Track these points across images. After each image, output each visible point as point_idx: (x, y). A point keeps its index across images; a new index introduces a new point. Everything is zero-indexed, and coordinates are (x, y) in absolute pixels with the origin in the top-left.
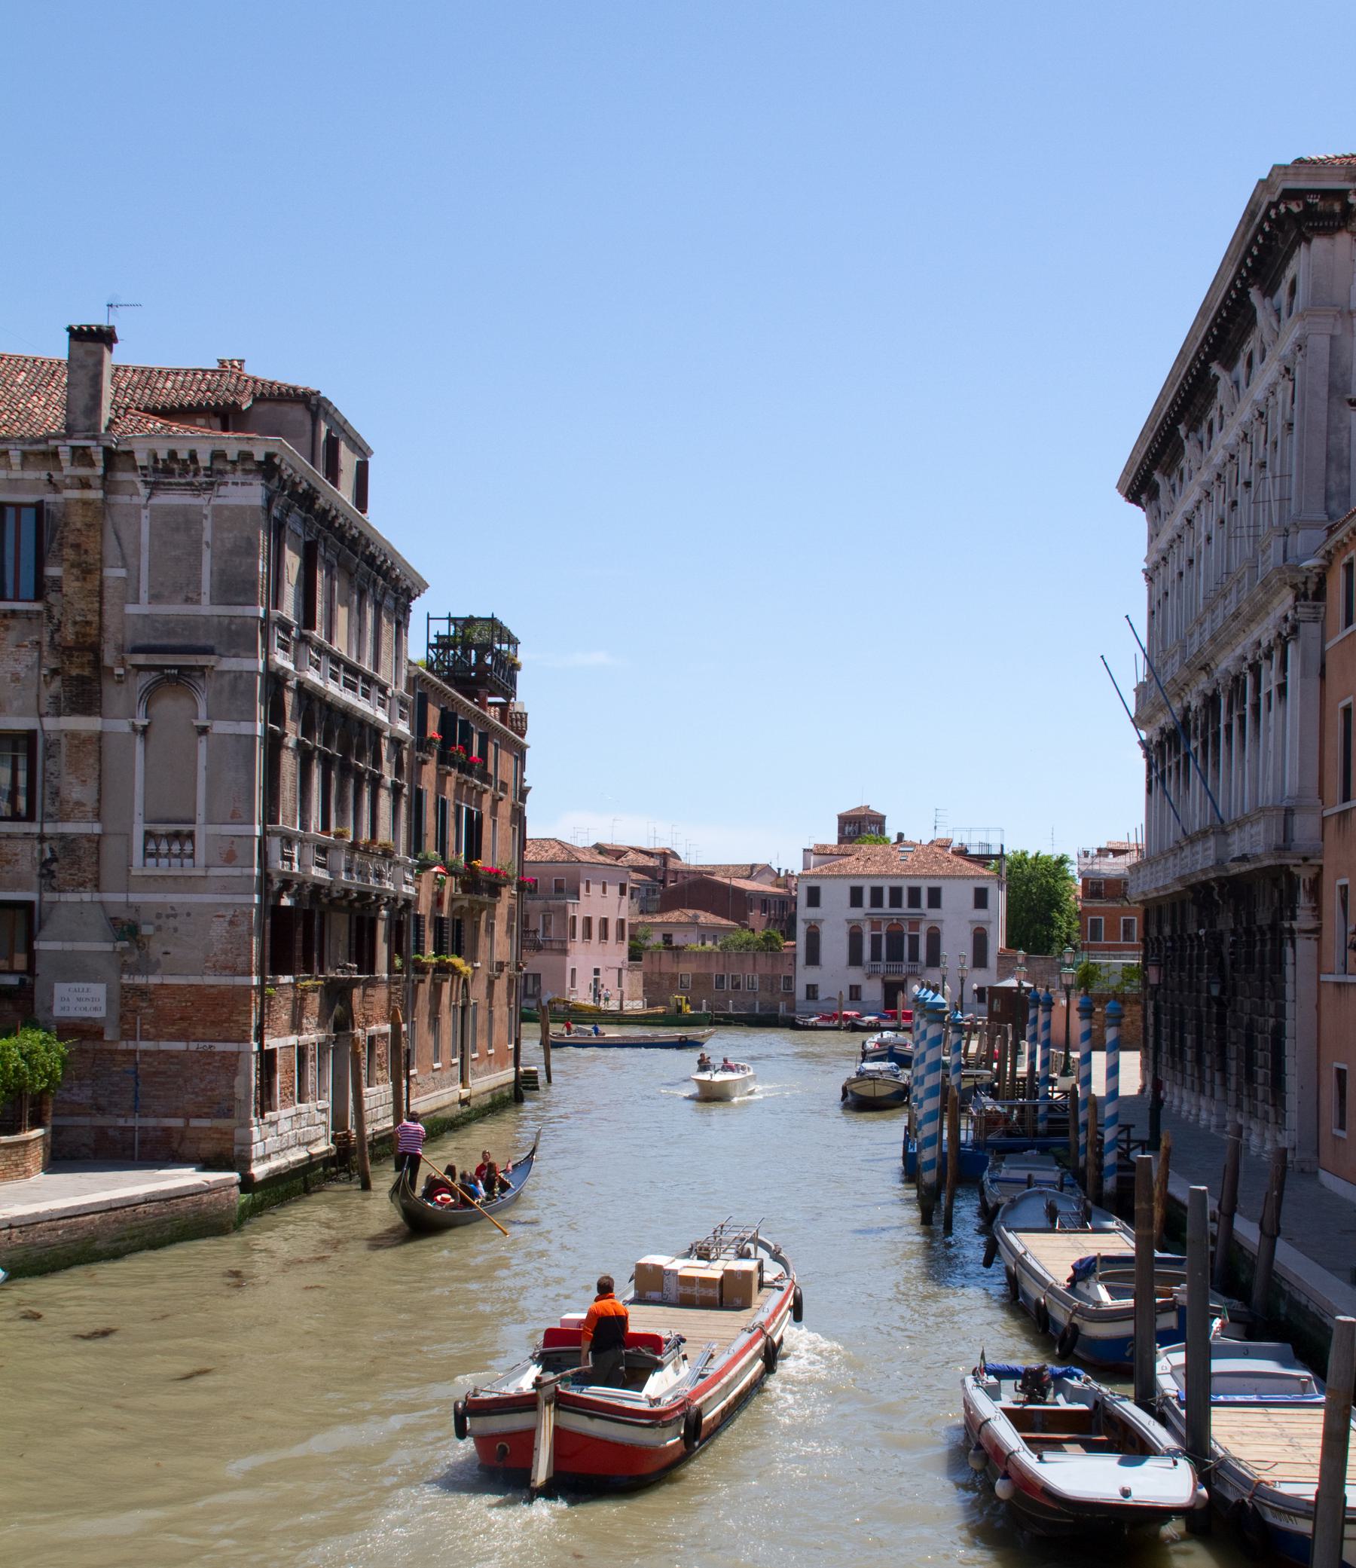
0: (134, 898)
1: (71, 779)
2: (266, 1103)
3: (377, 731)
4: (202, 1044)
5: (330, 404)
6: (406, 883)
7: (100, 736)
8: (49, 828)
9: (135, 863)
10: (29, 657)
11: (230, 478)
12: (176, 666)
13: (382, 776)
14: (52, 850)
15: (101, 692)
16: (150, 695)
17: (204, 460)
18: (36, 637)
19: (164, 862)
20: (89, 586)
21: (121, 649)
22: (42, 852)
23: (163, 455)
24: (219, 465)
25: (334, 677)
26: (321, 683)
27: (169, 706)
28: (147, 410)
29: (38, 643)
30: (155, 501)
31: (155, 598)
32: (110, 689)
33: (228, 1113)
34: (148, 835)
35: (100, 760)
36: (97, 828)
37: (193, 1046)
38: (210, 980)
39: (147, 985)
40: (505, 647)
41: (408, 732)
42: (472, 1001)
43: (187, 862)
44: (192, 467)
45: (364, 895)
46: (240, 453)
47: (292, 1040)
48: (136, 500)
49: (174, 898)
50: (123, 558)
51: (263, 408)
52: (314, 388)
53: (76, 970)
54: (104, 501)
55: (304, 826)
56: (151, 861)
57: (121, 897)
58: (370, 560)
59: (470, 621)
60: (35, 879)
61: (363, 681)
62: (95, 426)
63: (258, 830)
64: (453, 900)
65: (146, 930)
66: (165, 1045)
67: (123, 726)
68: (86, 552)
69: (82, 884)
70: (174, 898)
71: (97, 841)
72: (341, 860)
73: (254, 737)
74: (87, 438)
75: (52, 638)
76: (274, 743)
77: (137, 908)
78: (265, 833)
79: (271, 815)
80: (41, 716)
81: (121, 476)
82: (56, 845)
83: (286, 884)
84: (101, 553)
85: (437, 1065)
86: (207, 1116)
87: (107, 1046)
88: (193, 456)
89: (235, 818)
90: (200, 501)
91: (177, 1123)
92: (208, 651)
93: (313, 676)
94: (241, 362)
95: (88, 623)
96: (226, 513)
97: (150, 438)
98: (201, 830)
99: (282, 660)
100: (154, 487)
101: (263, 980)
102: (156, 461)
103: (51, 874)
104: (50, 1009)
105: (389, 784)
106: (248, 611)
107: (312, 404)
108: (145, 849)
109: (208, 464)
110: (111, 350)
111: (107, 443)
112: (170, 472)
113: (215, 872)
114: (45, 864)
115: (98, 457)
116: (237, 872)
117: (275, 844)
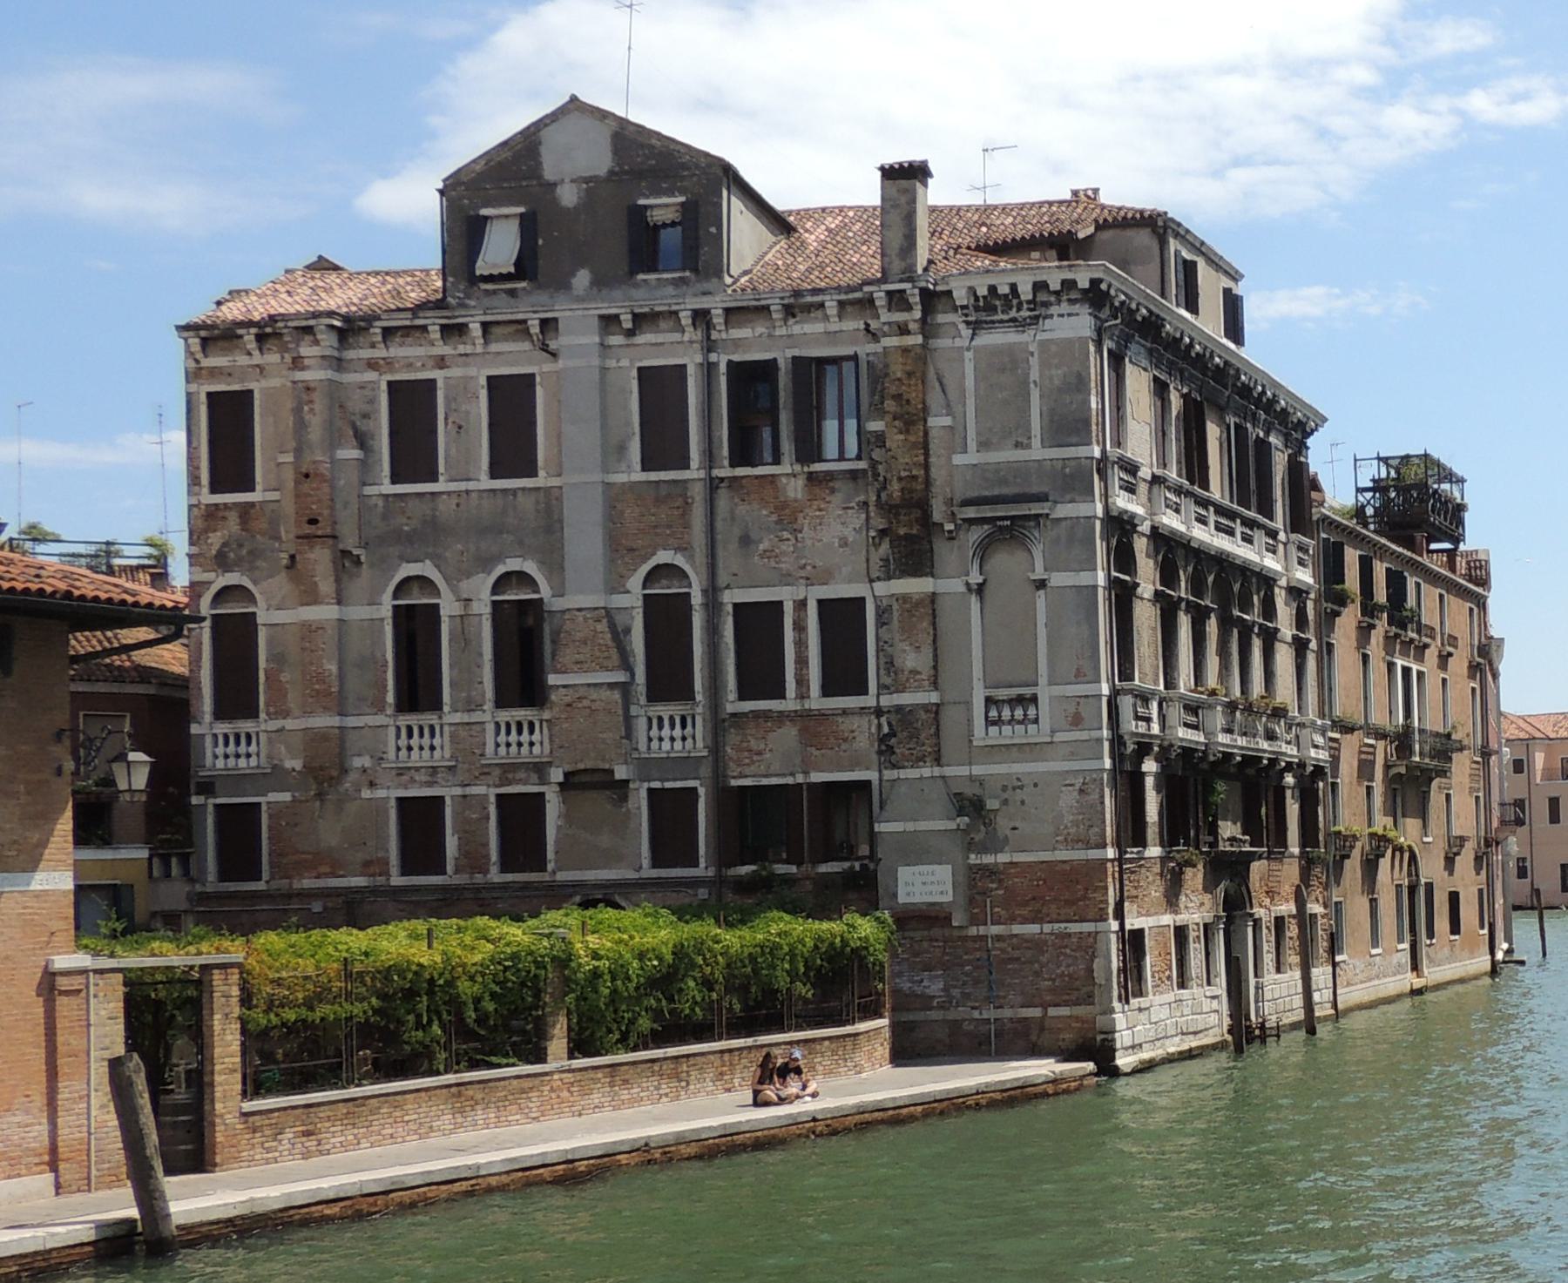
0: (977, 770)
1: (905, 646)
2: (1133, 980)
3: (1266, 581)
4: (1056, 926)
5: (1179, 225)
6: (1316, 747)
7: (933, 597)
8: (886, 701)
9: (976, 732)
10: (857, 519)
11: (1054, 310)
12: (1009, 519)
13: (1277, 630)
14: (889, 724)
15: (932, 550)
16: (984, 551)
17: (1026, 291)
18: (862, 498)
19: (1007, 729)
20: (912, 438)
21: (950, 502)
22: (879, 726)
23: (982, 291)
24: (1042, 297)
25: (1202, 520)
26: (1182, 528)
27: (1005, 561)
28: (978, 248)
29: (866, 503)
30: (978, 341)
31: (984, 445)
32: (941, 547)
33: (1089, 999)
34: (989, 701)
35: (934, 624)
36: (934, 697)
37: (1047, 928)
38: (1063, 855)
39: (996, 864)
40: (1446, 486)
41: (1311, 581)
42: (1423, 881)
43: (1032, 728)
44: (1015, 302)
45: (1251, 760)
46: (1063, 282)
47: (1167, 919)
48: (958, 342)
49: (1018, 768)
50: (948, 405)
51: (1106, 235)
52: (1161, 209)
53: (918, 851)
54: (924, 346)
55: (1170, 684)
56: (993, 730)
57: (963, 771)
58: (1245, 391)
59: (1406, 459)
60: (875, 757)
61: (1243, 524)
62: (911, 268)
63: (1105, 689)
64: (1387, 767)
65: (992, 804)
66: (1017, 929)
67: (955, 585)
68: (908, 401)
69: (922, 759)
70: (1018, 768)
71: (936, 710)
72: (1218, 718)
73: (1095, 587)
74: (901, 281)
75: (879, 496)
76: (1123, 596)
77: (980, 781)
78: (1115, 693)
79: (1126, 672)
80: (871, 581)
81: (941, 318)
82: (894, 718)
83: (1143, 749)
84: (924, 403)
85: (1374, 951)
86: (1066, 1004)
87: (956, 933)
88: (1014, 287)
89: (1079, 676)
90: (1026, 337)
91: (1035, 1012)
92: (1041, 498)
93: (1170, 521)
94: (1096, 191)
95: (914, 478)
96: (1054, 348)
97: (969, 278)
98: (1044, 692)
99: (1123, 501)
100: (976, 327)
101: (1122, 852)
102: (977, 299)
103: (891, 749)
104: (895, 895)
105: (1289, 639)
106: (1082, 451)
107: (1157, 226)
108: (987, 717)
109: (1030, 297)
110: (926, 185)
111: (923, 284)
112: (991, 309)
113: (1059, 737)
114: (883, 740)
115: (915, 299)
116: (1084, 735)
117: (1126, 703)
